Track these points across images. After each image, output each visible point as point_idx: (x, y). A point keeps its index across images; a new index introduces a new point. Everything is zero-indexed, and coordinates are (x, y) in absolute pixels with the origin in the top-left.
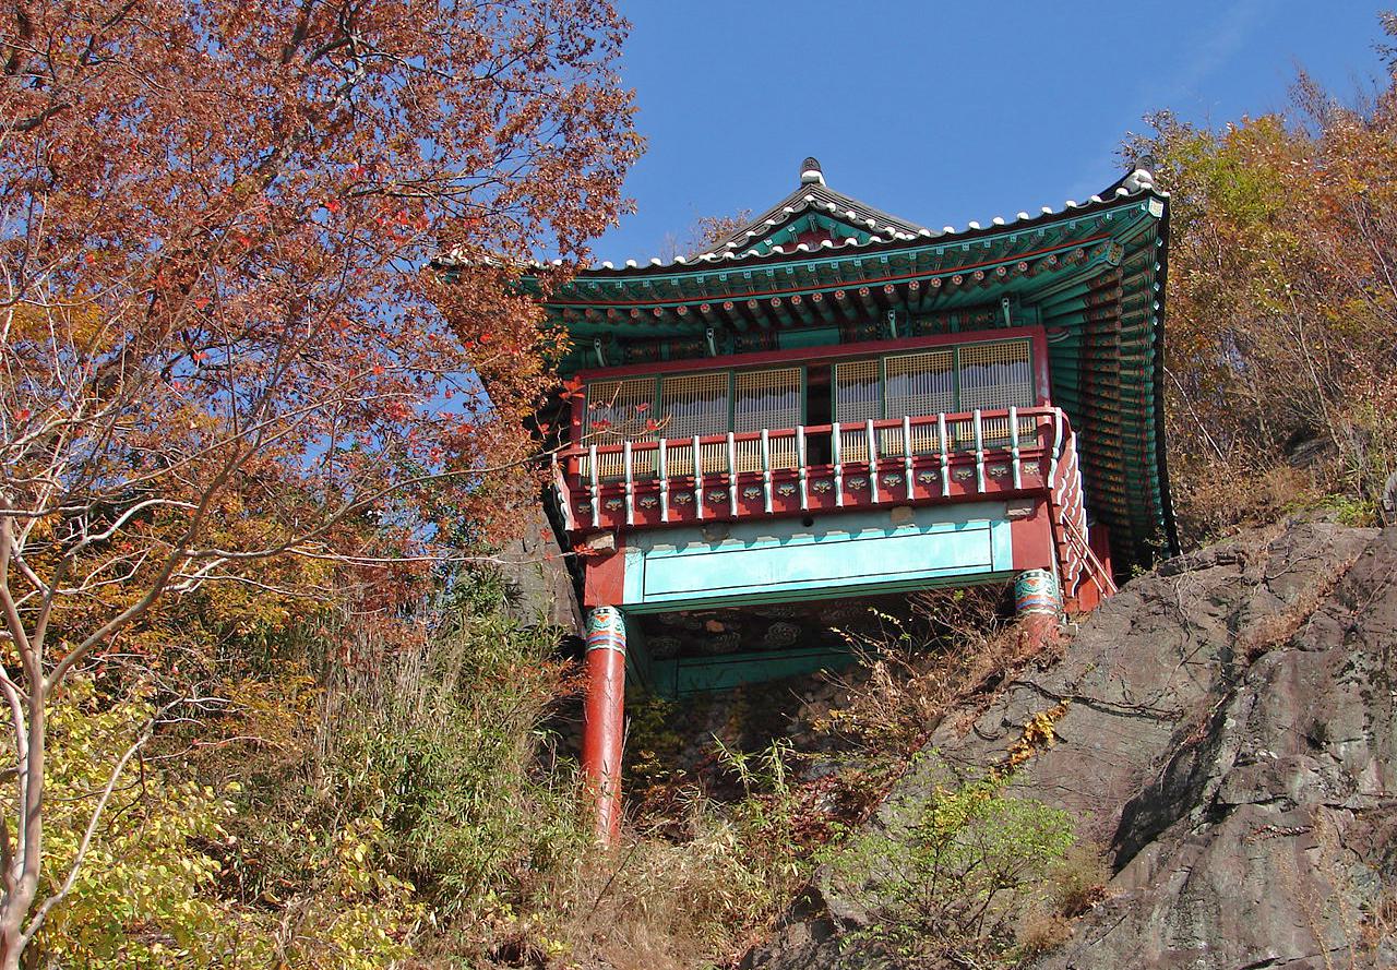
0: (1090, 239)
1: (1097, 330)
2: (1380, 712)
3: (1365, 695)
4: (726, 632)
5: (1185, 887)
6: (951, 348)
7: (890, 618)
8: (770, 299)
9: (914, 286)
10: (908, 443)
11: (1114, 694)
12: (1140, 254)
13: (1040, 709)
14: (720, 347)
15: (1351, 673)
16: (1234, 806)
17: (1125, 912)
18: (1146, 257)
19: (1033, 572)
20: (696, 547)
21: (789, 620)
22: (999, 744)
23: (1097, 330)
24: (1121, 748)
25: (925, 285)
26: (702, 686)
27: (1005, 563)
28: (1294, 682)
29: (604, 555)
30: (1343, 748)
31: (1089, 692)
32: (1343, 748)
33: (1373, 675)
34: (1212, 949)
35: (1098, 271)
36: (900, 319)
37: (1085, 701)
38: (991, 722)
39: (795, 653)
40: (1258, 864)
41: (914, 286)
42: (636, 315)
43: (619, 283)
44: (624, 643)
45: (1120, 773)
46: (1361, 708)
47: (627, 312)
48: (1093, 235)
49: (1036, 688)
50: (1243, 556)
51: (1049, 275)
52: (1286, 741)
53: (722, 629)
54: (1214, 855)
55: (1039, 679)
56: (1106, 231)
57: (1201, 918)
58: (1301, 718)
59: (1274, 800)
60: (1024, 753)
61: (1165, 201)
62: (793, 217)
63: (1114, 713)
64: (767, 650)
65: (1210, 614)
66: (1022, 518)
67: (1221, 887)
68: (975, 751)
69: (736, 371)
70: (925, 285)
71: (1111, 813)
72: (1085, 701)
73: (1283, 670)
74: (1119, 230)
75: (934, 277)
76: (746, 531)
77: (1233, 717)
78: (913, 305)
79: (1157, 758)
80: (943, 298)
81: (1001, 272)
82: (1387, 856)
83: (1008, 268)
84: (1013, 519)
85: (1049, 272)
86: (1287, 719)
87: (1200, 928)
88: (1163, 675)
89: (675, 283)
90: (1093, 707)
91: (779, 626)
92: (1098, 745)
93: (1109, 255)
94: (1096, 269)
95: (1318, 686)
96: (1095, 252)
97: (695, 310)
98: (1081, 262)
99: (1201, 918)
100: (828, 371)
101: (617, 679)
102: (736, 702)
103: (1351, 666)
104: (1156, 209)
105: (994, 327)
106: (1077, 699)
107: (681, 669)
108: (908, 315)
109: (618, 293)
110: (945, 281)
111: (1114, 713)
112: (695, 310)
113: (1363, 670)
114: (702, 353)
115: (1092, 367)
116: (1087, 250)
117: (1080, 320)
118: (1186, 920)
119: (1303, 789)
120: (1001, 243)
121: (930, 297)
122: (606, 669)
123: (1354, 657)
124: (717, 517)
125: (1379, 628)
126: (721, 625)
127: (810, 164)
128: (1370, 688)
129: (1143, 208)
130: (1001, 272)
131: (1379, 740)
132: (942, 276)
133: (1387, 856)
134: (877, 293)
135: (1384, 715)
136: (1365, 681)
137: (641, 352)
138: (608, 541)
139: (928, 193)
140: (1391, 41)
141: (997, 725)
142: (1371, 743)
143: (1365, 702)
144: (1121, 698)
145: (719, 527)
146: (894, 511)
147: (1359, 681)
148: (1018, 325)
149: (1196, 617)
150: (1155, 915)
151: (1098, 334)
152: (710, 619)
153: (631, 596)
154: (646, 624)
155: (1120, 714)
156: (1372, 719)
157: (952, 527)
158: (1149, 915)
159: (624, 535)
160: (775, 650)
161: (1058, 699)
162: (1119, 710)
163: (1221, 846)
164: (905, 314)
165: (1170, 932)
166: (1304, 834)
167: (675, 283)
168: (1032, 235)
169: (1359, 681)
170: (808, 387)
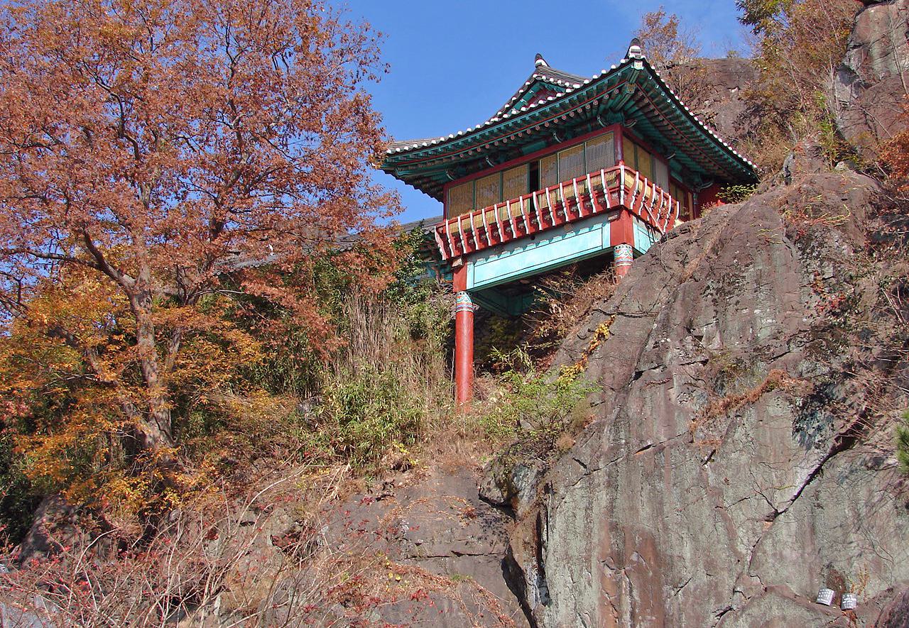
2: (720, 309)
3: (715, 301)
5: (618, 417)
6: (582, 143)
10: (576, 190)
11: (635, 308)
15: (708, 291)
16: (643, 372)
17: (594, 430)
19: (618, 247)
20: (480, 261)
22: (587, 341)
27: (607, 245)
28: (684, 300)
29: (459, 268)
30: (705, 329)
32: (705, 329)
33: (718, 290)
34: (627, 443)
37: (622, 314)
40: (648, 400)
42: (479, 150)
43: (477, 136)
46: (713, 308)
49: (601, 311)
52: (677, 331)
54: (629, 399)
57: (623, 429)
58: (685, 318)
59: (659, 366)
60: (596, 344)
61: (643, 60)
62: (530, 87)
63: (634, 317)
66: (614, 220)
67: (630, 414)
68: (578, 345)
72: (622, 314)
76: (510, 247)
82: (717, 381)
84: (611, 221)
86: (678, 321)
87: (622, 434)
89: (460, 143)
90: (625, 316)
92: (627, 334)
95: (694, 300)
99: (623, 429)
100: (537, 163)
101: (468, 322)
103: (708, 287)
104: (638, 66)
105: (597, 130)
106: (619, 314)
109: (450, 150)
110: (591, 104)
111: (634, 317)
113: (713, 288)
118: (617, 432)
119: (672, 359)
122: (462, 320)
123: (709, 283)
124: (499, 244)
125: (720, 267)
127: (538, 57)
128: (717, 297)
129: (632, 67)
131: (721, 322)
133: (717, 381)
135: (723, 310)
136: (714, 294)
138: (459, 262)
139: (581, 67)
141: (587, 331)
142: (717, 324)
143: (714, 305)
144: (638, 309)
145: (499, 248)
147: (712, 294)
148: (609, 125)
149: (669, 263)
150: (605, 430)
153: (469, 286)
154: (475, 294)
155: (637, 317)
156: (717, 312)
157: (587, 230)
158: (603, 430)
159: (466, 258)
161: (610, 315)
165: (612, 438)
166: (667, 381)
169: (712, 294)
170: (531, 172)
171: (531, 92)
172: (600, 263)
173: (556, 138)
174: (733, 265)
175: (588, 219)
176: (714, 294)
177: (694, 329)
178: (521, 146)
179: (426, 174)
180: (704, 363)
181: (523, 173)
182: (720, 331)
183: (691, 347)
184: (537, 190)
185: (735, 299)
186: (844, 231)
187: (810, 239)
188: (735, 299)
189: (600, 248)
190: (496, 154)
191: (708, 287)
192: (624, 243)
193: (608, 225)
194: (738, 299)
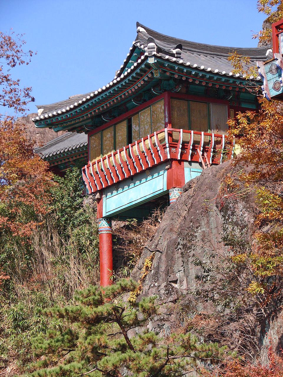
27: (165, 189)
28: (167, 253)
33: (184, 246)
43: (115, 88)
46: (181, 259)
72: (159, 251)
131: (186, 269)
135: (186, 260)
147: (181, 249)
153: (104, 215)
169: (181, 249)
171: (134, 54)
172: (161, 201)
173: (154, 92)
174: (190, 227)
175: (152, 170)
176: (182, 248)
177: (170, 276)
178: (125, 103)
179: (77, 125)
180: (174, 302)
181: (122, 129)
182: (186, 277)
183: (163, 291)
184: (131, 143)
185: (192, 252)
186: (247, 202)
187: (227, 209)
188: (192, 252)
189: (162, 191)
190: (108, 112)
191: (179, 244)
192: (175, 188)
193: (166, 172)
194: (194, 252)
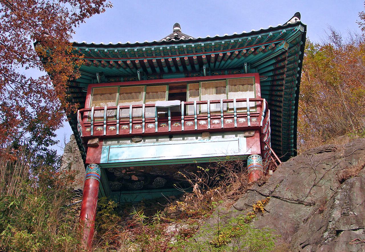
0: (277, 40)
1: (277, 78)
4: (139, 180)
6: (225, 79)
7: (201, 168)
8: (160, 59)
9: (213, 56)
11: (289, 195)
12: (293, 57)
13: (259, 200)
14: (142, 78)
18: (296, 49)
21: (162, 177)
23: (277, 78)
24: (291, 216)
25: (217, 56)
26: (129, 201)
29: (95, 146)
31: (277, 195)
35: (280, 52)
36: (207, 70)
37: (277, 197)
38: (240, 203)
39: (163, 190)
41: (213, 56)
44: (100, 175)
45: (290, 225)
47: (108, 62)
48: (277, 39)
50: (335, 149)
51: (261, 55)
53: (137, 179)
55: (259, 189)
56: (283, 37)
64: (154, 189)
65: (323, 169)
69: (147, 86)
70: (217, 56)
71: (286, 239)
72: (277, 197)
73: (357, 184)
74: (286, 38)
75: (220, 53)
77: (338, 200)
78: (212, 65)
79: (305, 220)
80: (223, 62)
81: (245, 52)
83: (247, 50)
85: (262, 53)
88: (306, 189)
91: (158, 178)
93: (284, 46)
94: (279, 51)
96: (278, 45)
97: (133, 62)
98: (273, 49)
102: (141, 206)
107: (122, 195)
108: (210, 69)
111: (287, 201)
112: (133, 62)
114: (136, 79)
115: (274, 98)
116: (276, 44)
117: (271, 74)
120: (245, 40)
121: (219, 62)
126: (137, 177)
130: (245, 52)
132: (223, 53)
134: (200, 58)
137: (113, 80)
140: (363, 21)
146: (203, 133)
151: (276, 90)
152: (133, 175)
160: (156, 189)
162: (289, 201)
163: (338, 246)
164: (209, 68)
167: (126, 50)
168: (256, 37)
